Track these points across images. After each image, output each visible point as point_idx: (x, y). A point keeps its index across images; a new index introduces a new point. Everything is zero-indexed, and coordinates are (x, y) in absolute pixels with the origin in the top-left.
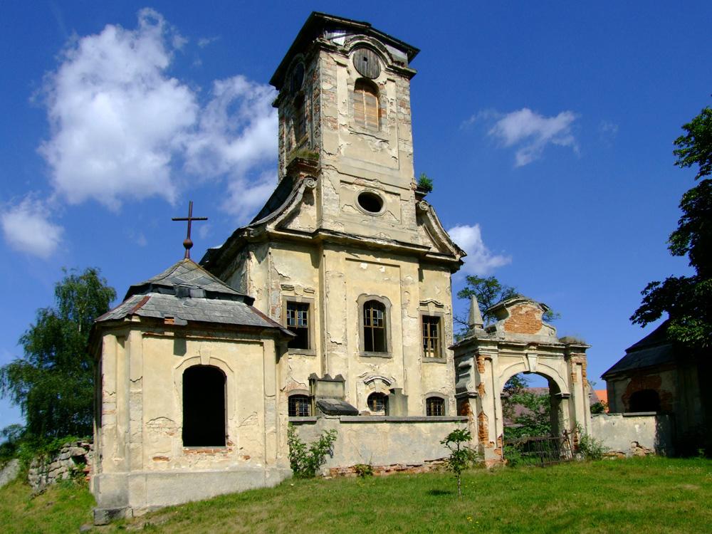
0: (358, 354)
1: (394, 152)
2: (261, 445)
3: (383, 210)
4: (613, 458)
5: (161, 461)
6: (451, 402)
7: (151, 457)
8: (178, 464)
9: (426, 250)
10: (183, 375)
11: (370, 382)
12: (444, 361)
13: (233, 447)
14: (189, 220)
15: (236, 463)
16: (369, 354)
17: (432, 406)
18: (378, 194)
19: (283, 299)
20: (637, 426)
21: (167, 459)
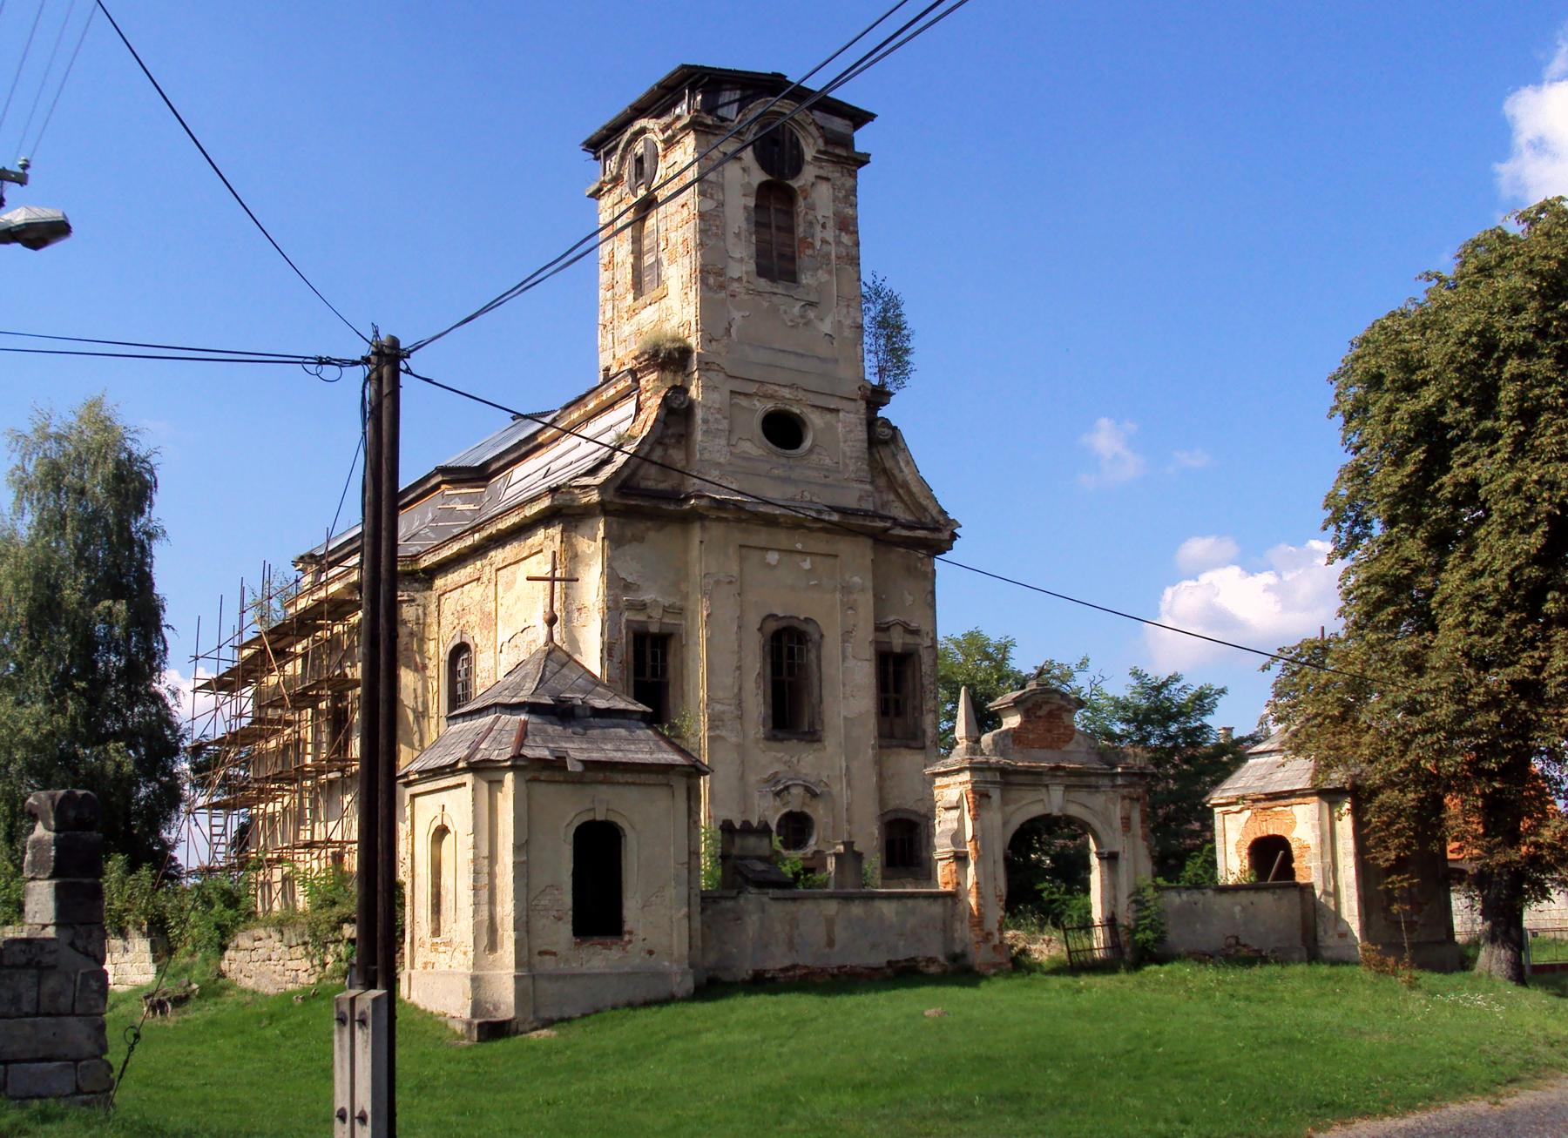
0: (761, 734)
1: (826, 327)
3: (807, 444)
5: (547, 957)
7: (536, 952)
8: (567, 961)
10: (575, 835)
11: (782, 791)
12: (921, 745)
15: (638, 961)
17: (891, 669)
18: (798, 412)
19: (628, 627)
20: (1237, 909)
21: (554, 954)
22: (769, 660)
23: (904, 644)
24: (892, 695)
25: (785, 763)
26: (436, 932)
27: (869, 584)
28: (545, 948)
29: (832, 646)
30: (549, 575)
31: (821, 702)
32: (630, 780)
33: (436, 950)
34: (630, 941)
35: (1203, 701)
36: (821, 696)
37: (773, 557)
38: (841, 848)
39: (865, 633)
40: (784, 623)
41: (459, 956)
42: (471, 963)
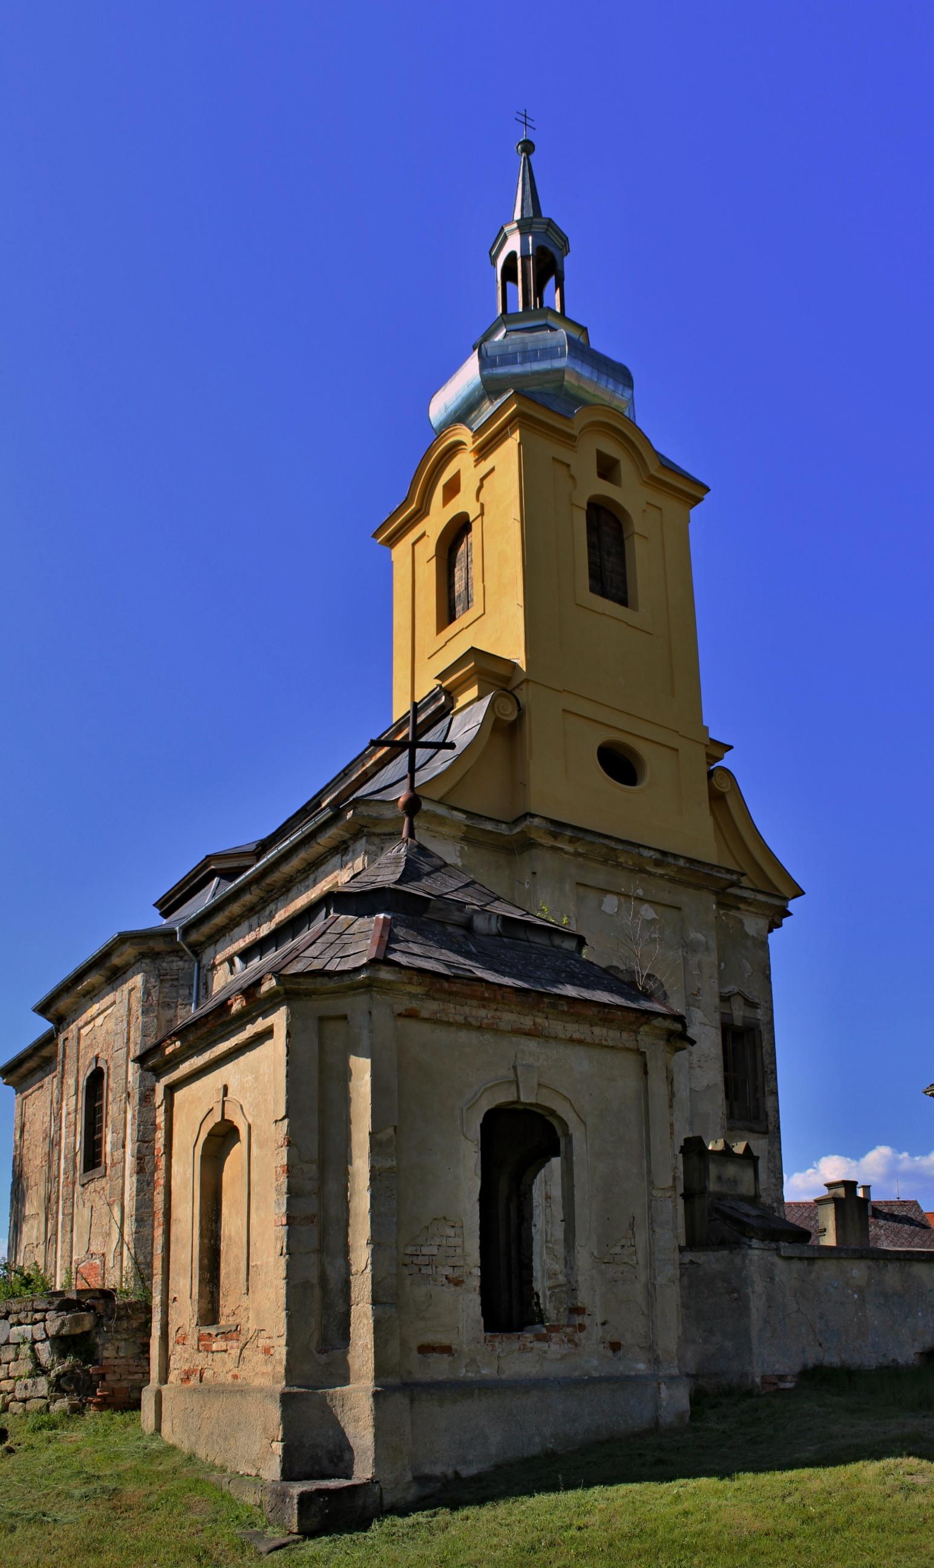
2: (643, 1314)
7: (414, 1346)
9: (735, 877)
10: (482, 1125)
13: (586, 1320)
21: (447, 1350)
23: (744, 1017)
26: (210, 1313)
27: (713, 944)
28: (430, 1338)
32: (576, 1036)
33: (208, 1350)
35: (480, 1508)
37: (611, 903)
41: (255, 1358)
42: (281, 1369)
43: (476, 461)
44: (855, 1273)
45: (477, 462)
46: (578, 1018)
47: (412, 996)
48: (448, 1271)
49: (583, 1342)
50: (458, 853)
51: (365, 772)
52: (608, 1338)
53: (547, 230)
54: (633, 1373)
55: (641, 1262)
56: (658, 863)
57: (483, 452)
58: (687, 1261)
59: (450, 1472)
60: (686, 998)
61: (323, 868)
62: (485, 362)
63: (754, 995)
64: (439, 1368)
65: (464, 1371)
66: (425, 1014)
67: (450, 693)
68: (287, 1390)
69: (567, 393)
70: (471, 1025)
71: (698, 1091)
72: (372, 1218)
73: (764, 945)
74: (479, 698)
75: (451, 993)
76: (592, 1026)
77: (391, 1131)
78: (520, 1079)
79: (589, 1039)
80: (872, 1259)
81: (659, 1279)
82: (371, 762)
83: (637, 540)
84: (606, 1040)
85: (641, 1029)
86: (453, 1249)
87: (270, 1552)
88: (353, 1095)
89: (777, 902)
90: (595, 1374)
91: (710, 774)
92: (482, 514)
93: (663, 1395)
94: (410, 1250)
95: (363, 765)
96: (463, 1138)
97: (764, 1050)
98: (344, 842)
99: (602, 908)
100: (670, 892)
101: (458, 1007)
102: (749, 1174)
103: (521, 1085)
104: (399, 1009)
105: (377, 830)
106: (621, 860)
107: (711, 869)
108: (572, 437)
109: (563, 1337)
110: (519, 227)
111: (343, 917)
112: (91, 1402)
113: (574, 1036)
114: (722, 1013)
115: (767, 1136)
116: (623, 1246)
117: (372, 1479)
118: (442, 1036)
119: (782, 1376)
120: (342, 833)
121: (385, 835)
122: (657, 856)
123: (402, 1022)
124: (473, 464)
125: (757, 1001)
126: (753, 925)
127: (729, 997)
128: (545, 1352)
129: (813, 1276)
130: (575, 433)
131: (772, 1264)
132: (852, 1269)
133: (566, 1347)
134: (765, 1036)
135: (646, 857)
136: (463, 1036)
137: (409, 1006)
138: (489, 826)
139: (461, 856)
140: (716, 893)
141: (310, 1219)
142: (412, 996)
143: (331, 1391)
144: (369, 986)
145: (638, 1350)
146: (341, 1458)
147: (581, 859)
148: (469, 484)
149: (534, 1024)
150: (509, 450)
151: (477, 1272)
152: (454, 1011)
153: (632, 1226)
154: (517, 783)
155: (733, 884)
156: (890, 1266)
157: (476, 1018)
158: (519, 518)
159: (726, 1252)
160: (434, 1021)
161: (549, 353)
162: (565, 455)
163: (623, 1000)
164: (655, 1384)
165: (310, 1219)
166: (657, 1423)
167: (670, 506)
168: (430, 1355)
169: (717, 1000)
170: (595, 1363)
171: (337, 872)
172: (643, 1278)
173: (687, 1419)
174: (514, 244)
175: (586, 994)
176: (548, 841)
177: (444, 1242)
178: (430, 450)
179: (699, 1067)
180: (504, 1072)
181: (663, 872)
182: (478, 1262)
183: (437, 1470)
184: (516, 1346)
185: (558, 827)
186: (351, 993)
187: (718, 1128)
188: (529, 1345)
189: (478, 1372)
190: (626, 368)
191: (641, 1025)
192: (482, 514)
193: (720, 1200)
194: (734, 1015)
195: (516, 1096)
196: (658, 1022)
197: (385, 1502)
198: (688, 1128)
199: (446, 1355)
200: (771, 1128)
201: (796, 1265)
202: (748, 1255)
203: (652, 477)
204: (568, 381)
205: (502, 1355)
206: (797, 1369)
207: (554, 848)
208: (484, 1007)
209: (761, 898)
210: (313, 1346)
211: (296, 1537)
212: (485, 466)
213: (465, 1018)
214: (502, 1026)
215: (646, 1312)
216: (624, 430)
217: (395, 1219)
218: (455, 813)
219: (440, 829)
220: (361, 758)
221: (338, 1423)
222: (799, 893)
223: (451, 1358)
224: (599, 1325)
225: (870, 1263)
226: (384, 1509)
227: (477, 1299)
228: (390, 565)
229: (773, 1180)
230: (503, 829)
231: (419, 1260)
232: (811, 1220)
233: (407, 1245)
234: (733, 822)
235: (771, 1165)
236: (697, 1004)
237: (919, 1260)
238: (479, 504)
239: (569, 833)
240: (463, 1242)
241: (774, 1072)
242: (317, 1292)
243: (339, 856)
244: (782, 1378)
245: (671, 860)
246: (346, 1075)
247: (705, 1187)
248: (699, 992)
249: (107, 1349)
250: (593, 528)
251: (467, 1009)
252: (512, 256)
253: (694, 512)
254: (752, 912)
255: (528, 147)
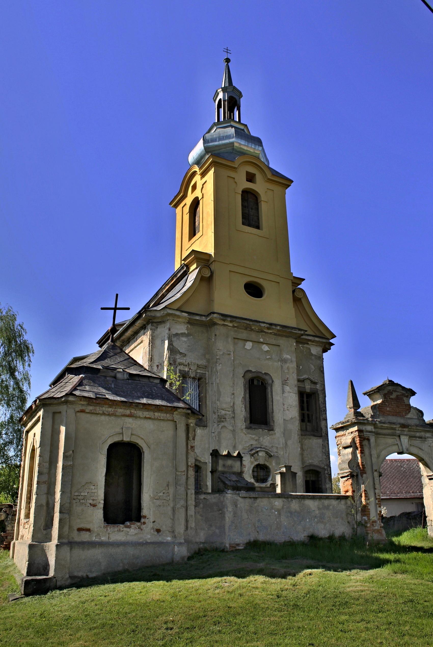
0: (244, 427)
2: (171, 519)
4: (295, 519)
6: (327, 475)
7: (75, 528)
9: (302, 332)
10: (108, 449)
11: (254, 453)
13: (146, 521)
14: (115, 309)
16: (253, 426)
17: (305, 399)
21: (89, 530)
22: (248, 391)
23: (311, 388)
24: (306, 412)
25: (256, 440)
27: (294, 359)
28: (82, 526)
29: (277, 387)
30: (117, 311)
31: (273, 412)
32: (148, 416)
34: (144, 523)
36: (273, 409)
37: (249, 345)
38: (284, 470)
39: (293, 379)
40: (254, 375)
43: (201, 178)
44: (276, 503)
45: (201, 178)
46: (148, 410)
47: (83, 405)
48: (91, 502)
49: (144, 529)
50: (186, 329)
51: (163, 294)
52: (155, 527)
53: (233, 90)
54: (165, 541)
55: (171, 499)
56: (268, 328)
57: (203, 175)
58: (203, 498)
59: (85, 575)
60: (282, 382)
61: (139, 335)
62: (205, 142)
63: (315, 378)
64: (85, 537)
65: (94, 538)
66: (87, 411)
67: (188, 266)
68: (31, 543)
69: (236, 151)
70: (105, 414)
71: (287, 420)
72: (62, 482)
73: (321, 359)
74: (196, 268)
75: (97, 403)
76: (154, 412)
77: (71, 452)
78: (124, 433)
79: (153, 417)
80: (285, 498)
81: (177, 505)
82: (164, 291)
83: (262, 203)
84: (160, 417)
85: (175, 413)
86: (93, 493)
87: (12, 601)
88: (60, 439)
89: (324, 341)
90: (149, 541)
91: (294, 291)
92: (203, 197)
93: (176, 550)
94: (76, 494)
95: (162, 292)
96: (100, 454)
97: (320, 402)
98: (144, 325)
99: (245, 347)
100: (275, 339)
101: (100, 408)
102: (238, 463)
103: (124, 434)
104: (77, 409)
105: (155, 321)
106: (253, 328)
107: (292, 329)
108: (235, 168)
109: (136, 527)
110: (222, 90)
111: (71, 375)
112: (1, 547)
113: (147, 416)
114: (298, 387)
115: (322, 438)
116: (164, 493)
117: (53, 576)
118: (94, 418)
119: (238, 544)
120: (143, 322)
121: (158, 322)
122: (268, 326)
123: (78, 414)
124: (200, 179)
125: (316, 381)
126: (315, 350)
127: (304, 380)
128: (128, 532)
129: (256, 504)
130: (236, 166)
131: (237, 500)
132: (275, 502)
133: (137, 530)
134: (321, 396)
135: (263, 327)
136: (103, 418)
137: (81, 408)
138: (198, 318)
139: (187, 330)
140: (295, 339)
141: (44, 482)
142: (83, 405)
143: (45, 544)
144: (66, 402)
145: (168, 532)
146: (46, 568)
147: (236, 329)
148: (199, 186)
149: (131, 413)
150: (211, 174)
151: (103, 502)
152: (99, 409)
153: (168, 485)
154: (210, 300)
155: (302, 335)
156: (294, 501)
157: (107, 411)
158: (213, 200)
159: (218, 495)
160: (91, 413)
161: (228, 137)
162: (232, 174)
163: (166, 403)
164: (173, 545)
165: (44, 482)
166: (173, 561)
167: (277, 189)
168: (81, 532)
169: (296, 382)
170: (149, 536)
171: (143, 336)
172: (172, 505)
173: (186, 559)
174: (221, 96)
175: (150, 402)
176: (222, 323)
177: (90, 491)
178: (187, 173)
179: (288, 410)
180: (118, 430)
181: (271, 331)
182: (103, 498)
183: (80, 574)
184: (116, 529)
185: (224, 316)
186: (62, 404)
187: (296, 435)
188: (121, 529)
189: (100, 539)
190: (260, 139)
191: (174, 411)
192: (203, 197)
193: (223, 474)
194: (306, 387)
195: (122, 438)
196: (179, 410)
197: (57, 585)
198: (282, 435)
199: (88, 532)
200: (323, 434)
201: (248, 500)
202: (226, 496)
203: (269, 179)
204: (236, 146)
205: (110, 533)
206: (245, 542)
207: (224, 325)
208: (110, 407)
209: (317, 339)
210: (42, 528)
211: (22, 596)
212: (204, 180)
213: (103, 412)
214: (117, 414)
215: (172, 518)
216: (257, 163)
217: (70, 483)
218: (183, 314)
219: (178, 319)
220: (161, 289)
221: (46, 555)
222: (334, 336)
223: (90, 533)
224: (152, 522)
225: (284, 499)
226: (57, 587)
227: (101, 512)
228: (175, 214)
229: (325, 457)
230: (204, 318)
231: (80, 497)
232: (402, 467)
233: (75, 492)
234: (305, 309)
235: (324, 450)
236: (287, 384)
237: (308, 498)
238: (202, 194)
239: (229, 319)
240: (97, 491)
241: (325, 411)
242: (45, 508)
243: (143, 330)
244: (238, 545)
245: (274, 327)
246: (59, 432)
247: (217, 469)
248: (287, 379)
249: (9, 527)
250: (244, 199)
251: (104, 408)
252: (220, 100)
253: (288, 191)
254: (314, 345)
255: (228, 60)
